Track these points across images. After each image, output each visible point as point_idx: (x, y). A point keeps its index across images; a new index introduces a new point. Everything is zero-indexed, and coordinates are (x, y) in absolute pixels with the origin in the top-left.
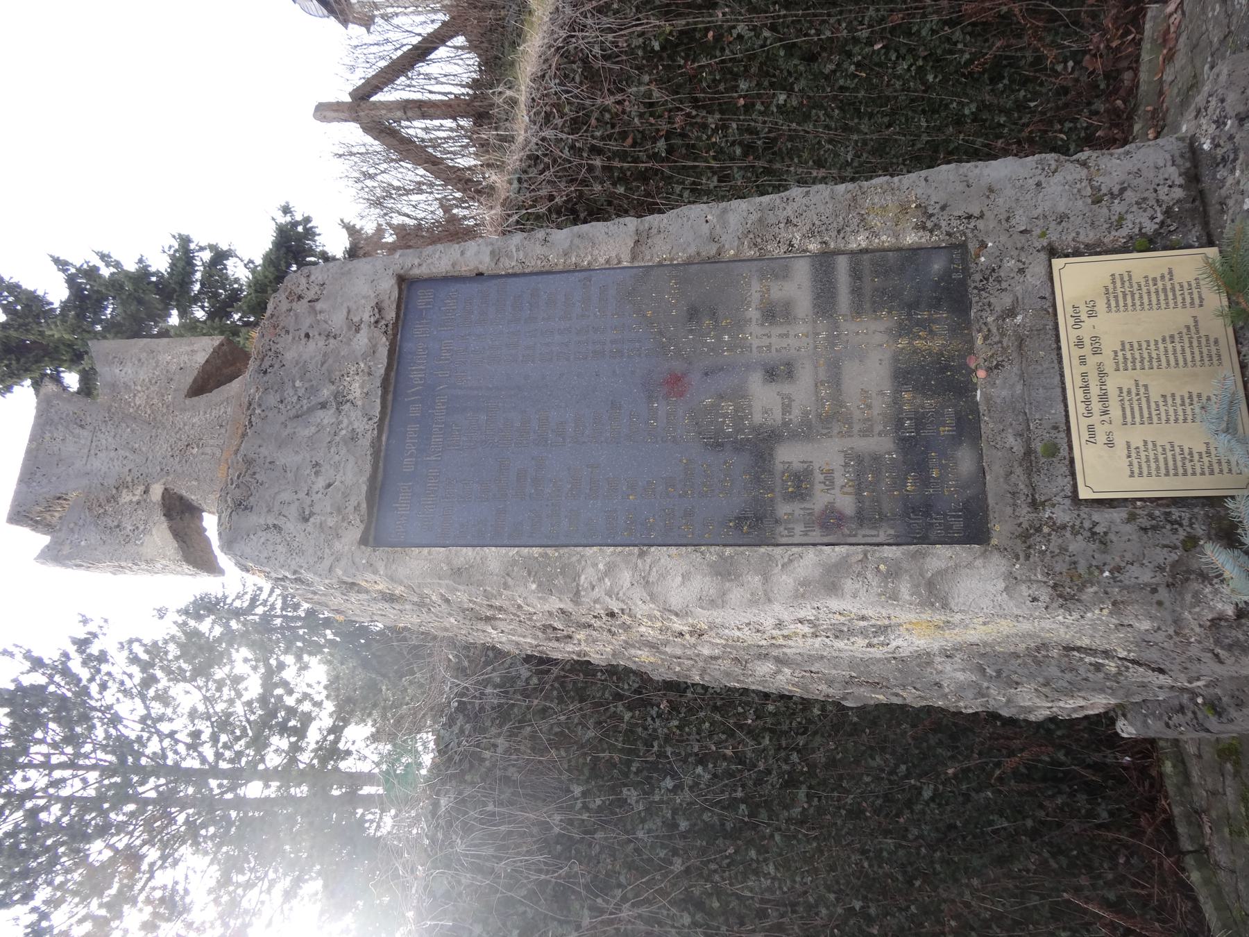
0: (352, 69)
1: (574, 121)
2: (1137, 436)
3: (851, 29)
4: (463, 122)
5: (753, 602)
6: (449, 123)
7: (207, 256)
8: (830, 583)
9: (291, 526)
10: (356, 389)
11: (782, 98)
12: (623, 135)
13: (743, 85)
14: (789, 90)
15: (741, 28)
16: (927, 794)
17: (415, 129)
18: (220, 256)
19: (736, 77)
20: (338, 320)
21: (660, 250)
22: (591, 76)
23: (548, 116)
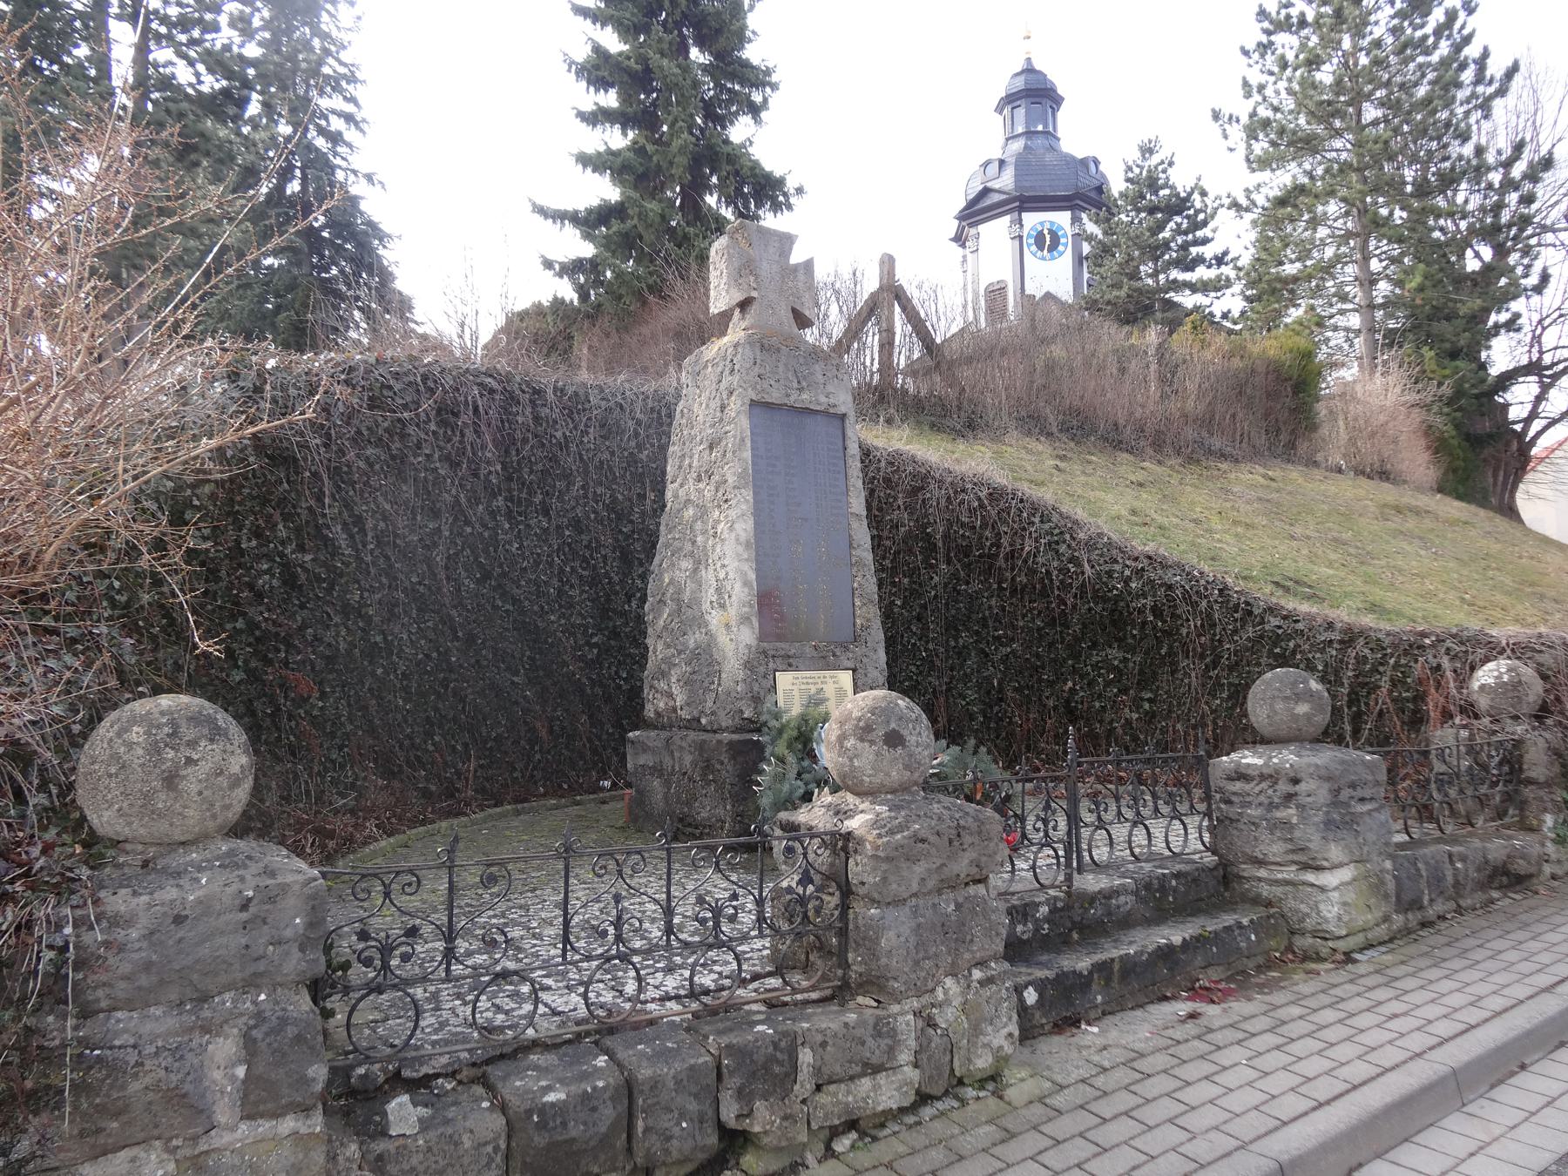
0: (920, 287)
1: (890, 480)
2: (796, 693)
3: (934, 639)
4: (876, 377)
5: (738, 555)
6: (876, 366)
7: (757, 97)
8: (746, 583)
9: (757, 370)
10: (805, 396)
11: (898, 603)
12: (880, 509)
13: (906, 581)
14: (902, 607)
15: (936, 579)
16: (516, 679)
17: (872, 339)
18: (755, 110)
19: (911, 576)
20: (830, 388)
21: (855, 525)
22: (915, 491)
23: (892, 464)
